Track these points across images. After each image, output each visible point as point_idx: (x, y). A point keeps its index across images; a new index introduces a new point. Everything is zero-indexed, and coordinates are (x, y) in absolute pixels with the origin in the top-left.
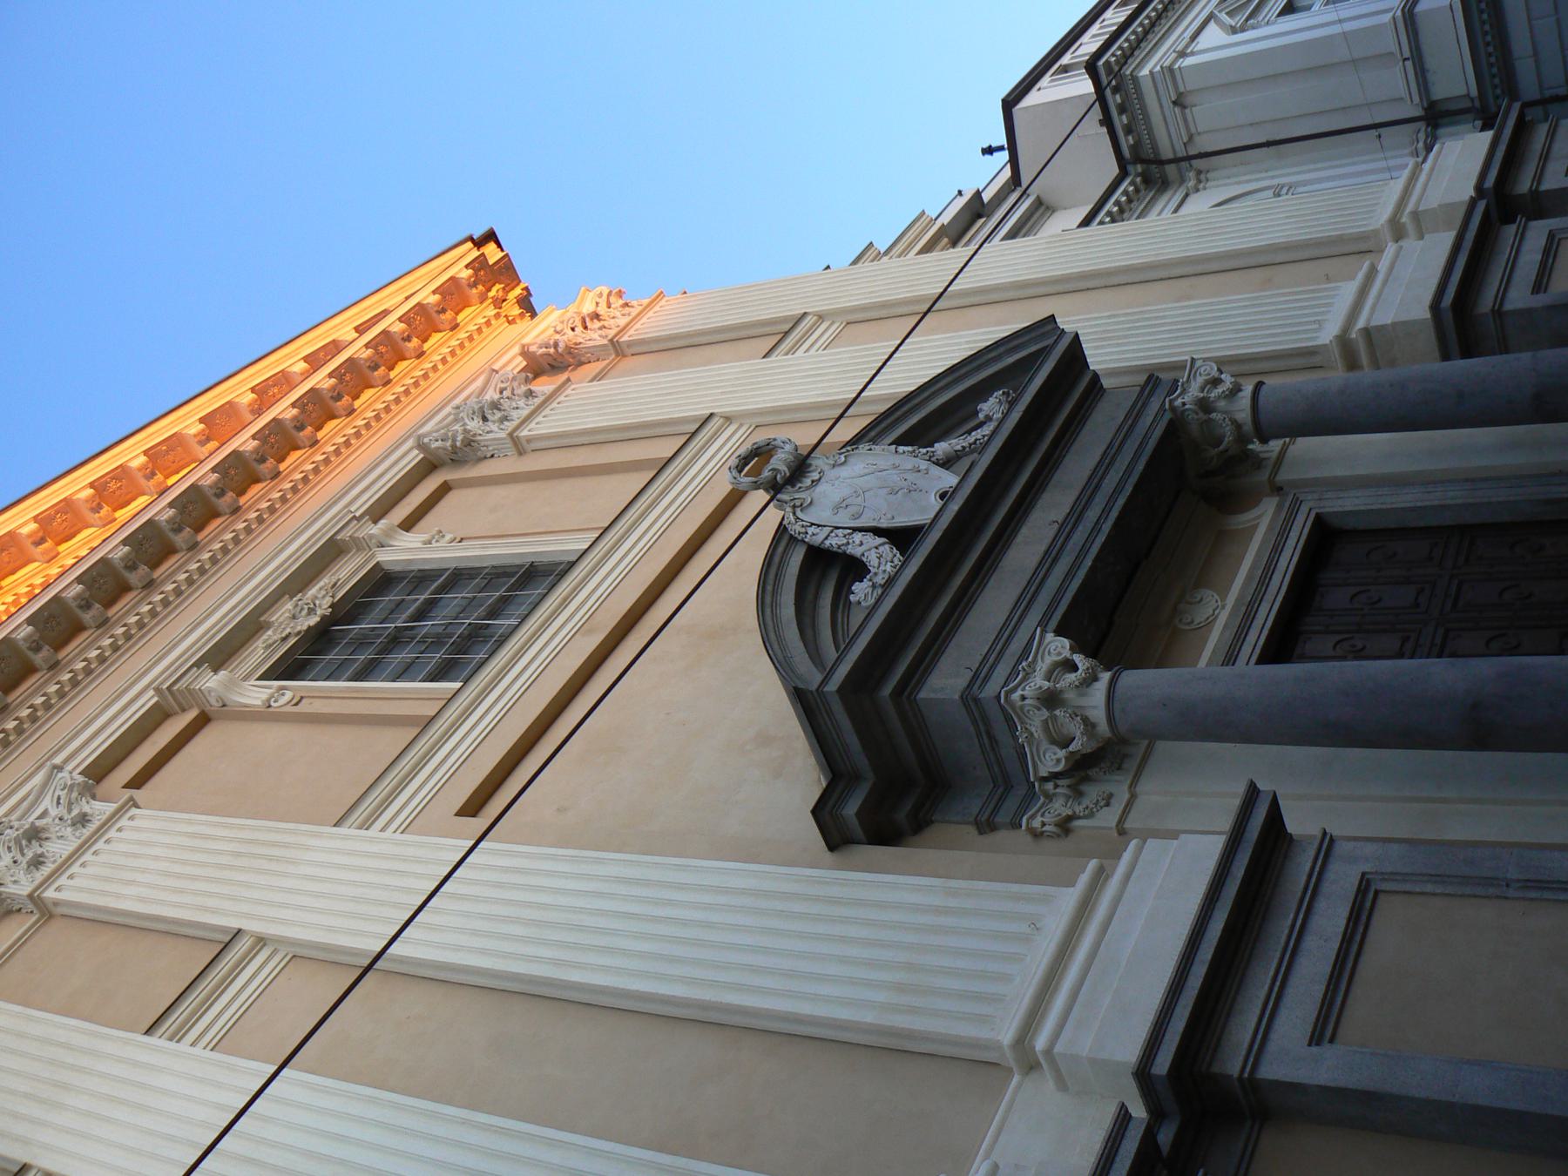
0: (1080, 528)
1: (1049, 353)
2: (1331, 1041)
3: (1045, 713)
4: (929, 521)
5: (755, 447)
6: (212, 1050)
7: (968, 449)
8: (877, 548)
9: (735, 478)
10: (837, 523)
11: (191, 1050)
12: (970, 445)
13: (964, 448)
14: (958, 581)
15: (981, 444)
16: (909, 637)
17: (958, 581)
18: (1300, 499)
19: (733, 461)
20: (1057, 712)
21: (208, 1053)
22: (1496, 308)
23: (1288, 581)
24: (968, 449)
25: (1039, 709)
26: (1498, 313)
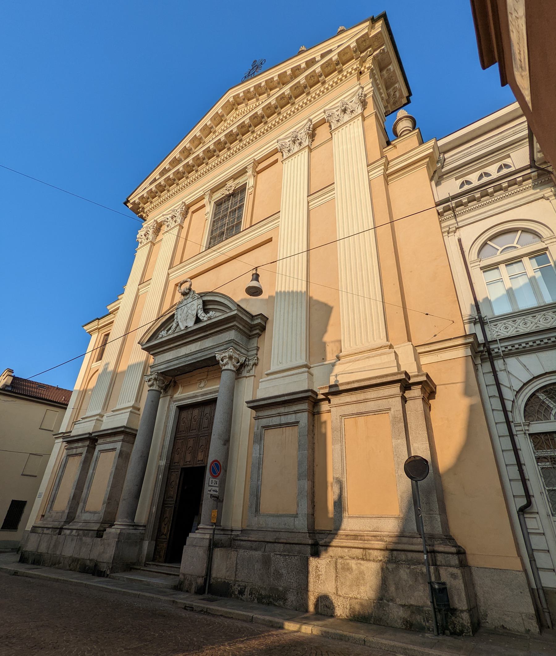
14: (172, 346)
16: (186, 338)
17: (172, 346)
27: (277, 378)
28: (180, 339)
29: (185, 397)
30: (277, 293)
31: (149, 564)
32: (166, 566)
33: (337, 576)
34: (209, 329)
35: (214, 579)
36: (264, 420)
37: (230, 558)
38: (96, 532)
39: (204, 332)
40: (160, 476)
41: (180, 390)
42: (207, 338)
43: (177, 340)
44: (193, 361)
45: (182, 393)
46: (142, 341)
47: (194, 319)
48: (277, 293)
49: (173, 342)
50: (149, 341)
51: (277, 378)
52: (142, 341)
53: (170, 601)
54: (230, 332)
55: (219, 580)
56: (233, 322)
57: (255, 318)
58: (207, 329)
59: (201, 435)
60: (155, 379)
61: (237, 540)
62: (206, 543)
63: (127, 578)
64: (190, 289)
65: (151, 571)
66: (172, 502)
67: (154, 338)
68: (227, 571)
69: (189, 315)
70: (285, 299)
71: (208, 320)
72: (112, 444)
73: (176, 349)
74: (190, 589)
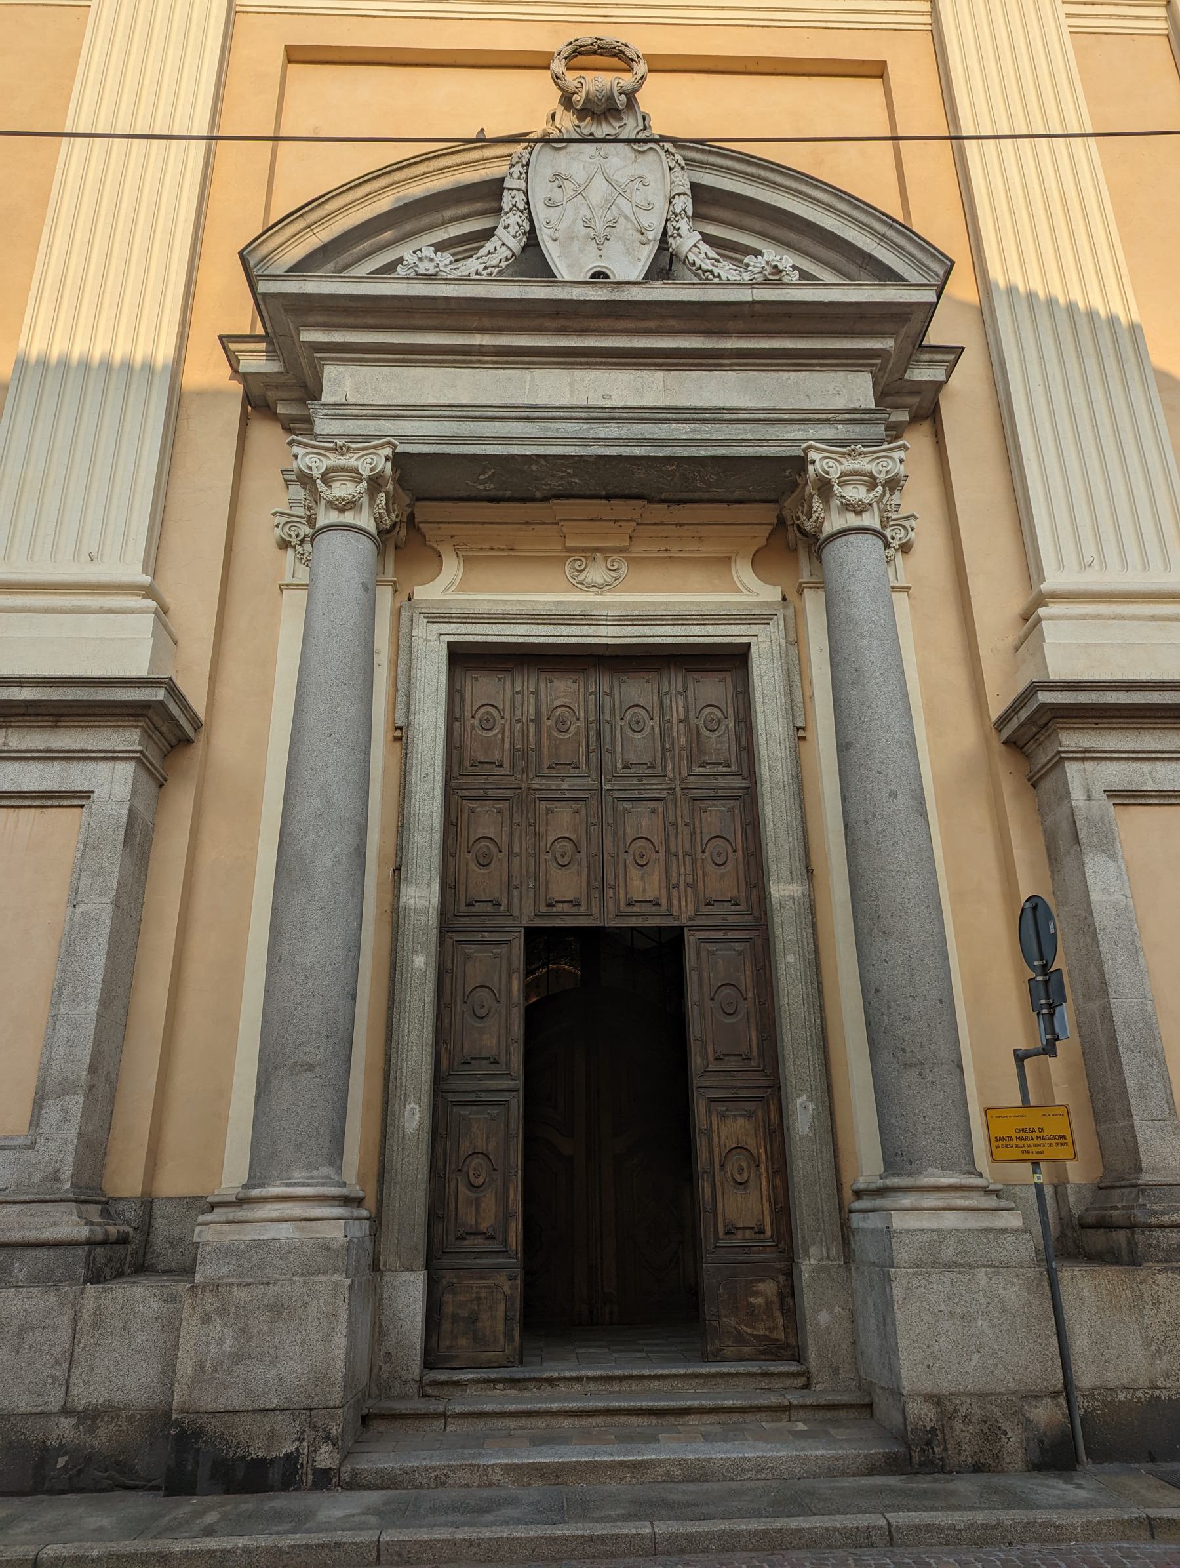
0: (586, 426)
1: (706, 283)
2: (166, 780)
3: (366, 474)
4: (559, 278)
5: (623, 48)
6: (1071, 33)
7: (694, 268)
8: (503, 244)
9: (559, 54)
10: (533, 191)
11: (1062, 17)
12: (700, 268)
13: (694, 264)
14: (478, 340)
15: (707, 279)
16: (583, 332)
17: (478, 340)
18: (771, 622)
19: (585, 35)
20: (365, 483)
21: (1066, 31)
22: (1063, 755)
23: (661, 642)
24: (694, 268)
25: (372, 470)
26: (1059, 760)
27: (1123, 618)
28: (548, 323)
29: (513, 610)
30: (22, 364)
31: (457, 1383)
32: (589, 1379)
33: (854, 1343)
34: (741, 325)
35: (1090, 1395)
36: (1113, 767)
37: (1155, 1303)
38: (81, 1252)
39: (707, 333)
40: (420, 961)
41: (452, 569)
42: (711, 368)
43: (525, 323)
44: (638, 451)
45: (459, 590)
46: (264, 250)
47: (647, 254)
48: (22, 364)
49: (501, 323)
50: (301, 267)
51: (1123, 618)
52: (264, 250)
53: (1130, 1522)
54: (851, 376)
55: (1122, 1397)
56: (882, 334)
57: (926, 357)
58: (731, 325)
59: (617, 794)
60: (375, 483)
61: (1162, 1227)
62: (1024, 1248)
63: (507, 1469)
64: (630, 96)
65: (480, 1415)
66: (504, 1084)
67: (331, 266)
68: (1158, 1353)
69: (622, 220)
70: (37, 407)
71: (767, 282)
72: (57, 766)
73: (498, 365)
74: (997, 1457)
